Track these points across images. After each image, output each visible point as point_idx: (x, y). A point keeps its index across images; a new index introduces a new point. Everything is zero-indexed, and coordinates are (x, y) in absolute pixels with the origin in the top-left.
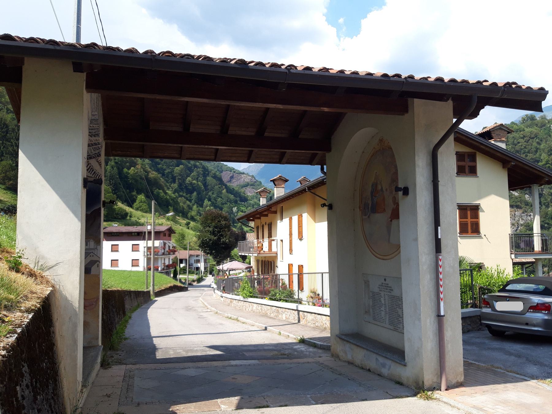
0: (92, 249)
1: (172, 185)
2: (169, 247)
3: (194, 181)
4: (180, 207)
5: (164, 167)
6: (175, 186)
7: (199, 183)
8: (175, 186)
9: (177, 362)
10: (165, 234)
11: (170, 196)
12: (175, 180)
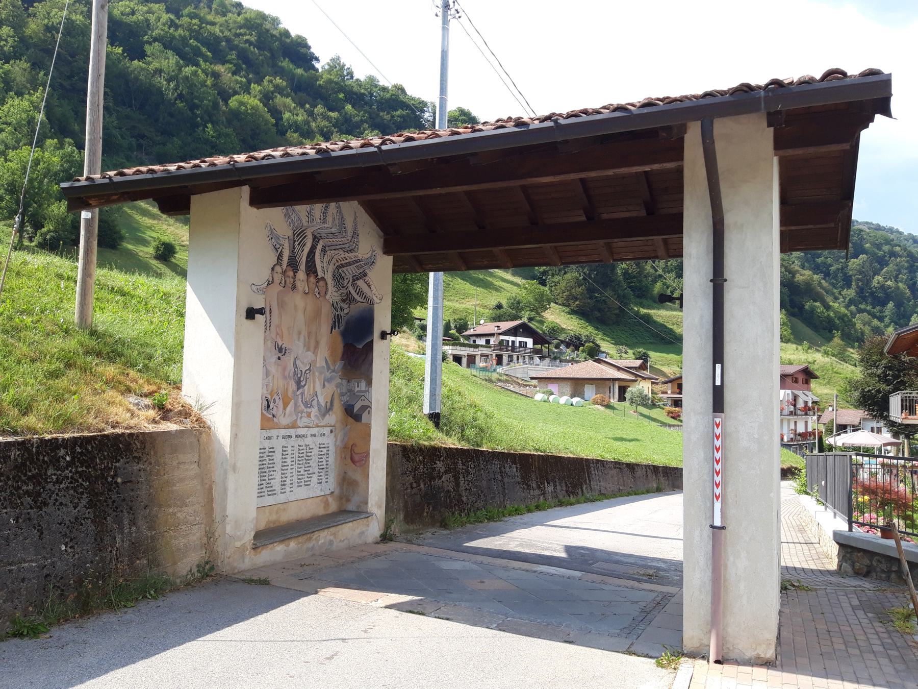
0: (363, 392)
1: (845, 292)
2: (806, 402)
3: (889, 283)
4: (856, 330)
5: (829, 261)
6: (851, 293)
7: (900, 284)
8: (851, 293)
9: (474, 553)
10: (796, 378)
11: (836, 312)
12: (851, 282)
